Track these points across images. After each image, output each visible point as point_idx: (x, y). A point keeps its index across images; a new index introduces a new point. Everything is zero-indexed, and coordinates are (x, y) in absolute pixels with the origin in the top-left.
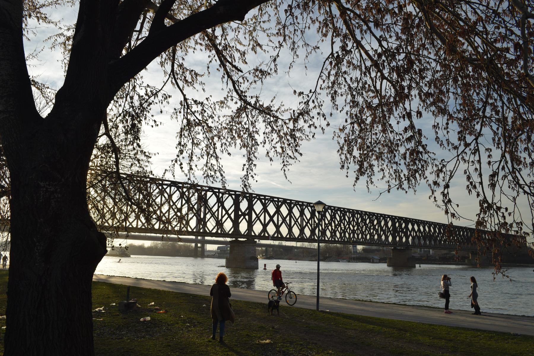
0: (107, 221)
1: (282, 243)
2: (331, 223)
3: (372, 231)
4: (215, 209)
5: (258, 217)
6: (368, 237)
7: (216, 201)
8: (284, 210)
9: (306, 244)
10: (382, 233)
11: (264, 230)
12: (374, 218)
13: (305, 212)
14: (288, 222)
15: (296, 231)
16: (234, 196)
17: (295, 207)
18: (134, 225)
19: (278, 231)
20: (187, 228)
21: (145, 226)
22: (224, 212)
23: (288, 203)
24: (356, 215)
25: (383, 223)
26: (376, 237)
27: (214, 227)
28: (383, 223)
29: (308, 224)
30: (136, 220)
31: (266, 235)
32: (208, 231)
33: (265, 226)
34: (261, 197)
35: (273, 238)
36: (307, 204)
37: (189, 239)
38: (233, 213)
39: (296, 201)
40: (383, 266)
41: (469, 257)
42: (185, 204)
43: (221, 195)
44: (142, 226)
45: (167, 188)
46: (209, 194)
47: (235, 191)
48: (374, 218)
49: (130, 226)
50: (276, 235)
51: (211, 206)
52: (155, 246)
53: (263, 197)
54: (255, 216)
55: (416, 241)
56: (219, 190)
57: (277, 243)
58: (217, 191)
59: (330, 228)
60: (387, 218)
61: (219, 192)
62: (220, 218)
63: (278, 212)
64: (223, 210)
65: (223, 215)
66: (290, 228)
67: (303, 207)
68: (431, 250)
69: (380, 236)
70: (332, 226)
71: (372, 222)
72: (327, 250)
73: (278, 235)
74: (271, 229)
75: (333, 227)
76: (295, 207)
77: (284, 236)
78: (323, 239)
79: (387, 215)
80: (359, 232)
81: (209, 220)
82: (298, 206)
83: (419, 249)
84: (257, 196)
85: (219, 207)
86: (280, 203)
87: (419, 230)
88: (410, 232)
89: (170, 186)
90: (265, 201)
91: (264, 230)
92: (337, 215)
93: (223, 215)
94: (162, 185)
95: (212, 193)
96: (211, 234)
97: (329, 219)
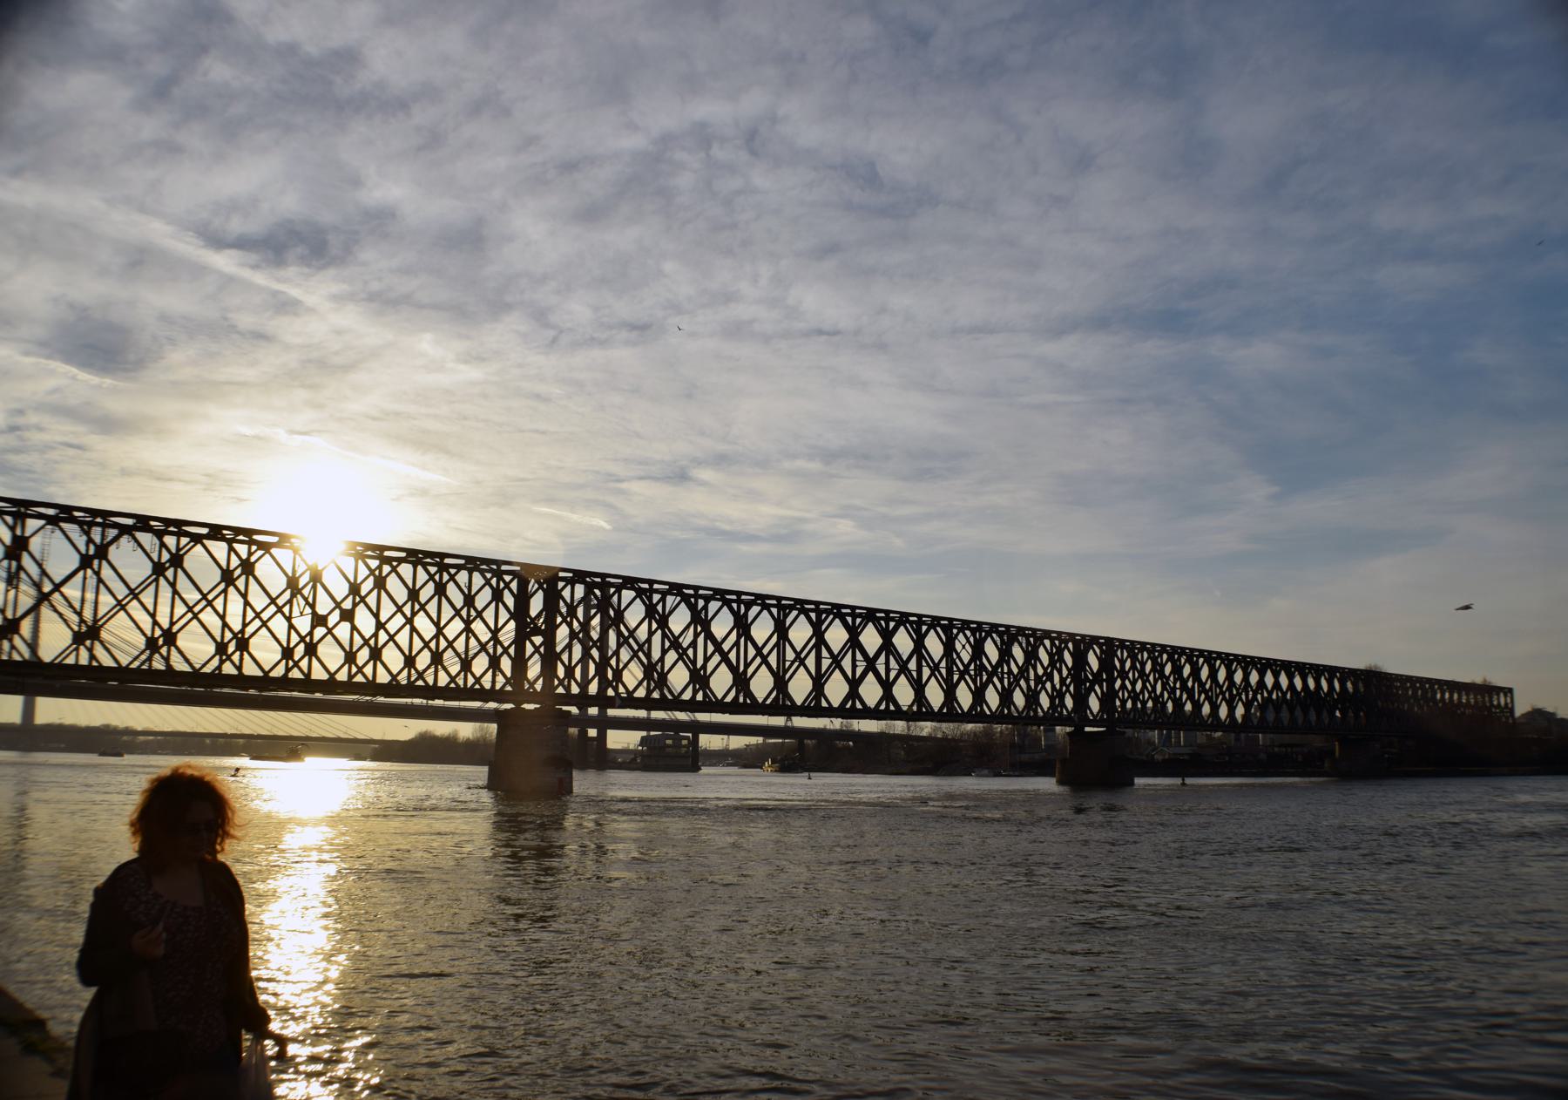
0: (360, 670)
1: (852, 725)
3: (1178, 692)
4: (642, 634)
6: (1150, 704)
8: (903, 641)
9: (899, 726)
11: (853, 694)
12: (1183, 661)
13: (461, 598)
15: (935, 695)
16: (813, 615)
17: (932, 631)
18: (487, 682)
19: (888, 696)
20: (616, 689)
22: (711, 648)
23: (911, 623)
24: (1119, 653)
25: (1205, 673)
26: (1188, 707)
28: (1205, 673)
29: (995, 680)
30: (307, 657)
31: (859, 706)
32: (988, 713)
33: (854, 683)
34: (844, 611)
38: (814, 650)
39: (934, 618)
40: (1047, 784)
41: (1333, 753)
42: (656, 630)
45: (511, 581)
46: (628, 595)
47: (779, 599)
48: (1183, 661)
49: (420, 683)
50: (883, 707)
51: (633, 625)
52: (482, 736)
53: (849, 611)
54: (843, 663)
55: (1271, 716)
56: (651, 586)
58: (692, 592)
59: (1048, 685)
60: (1198, 657)
62: (742, 668)
63: (888, 647)
65: (734, 651)
66: (919, 687)
67: (980, 635)
68: (1260, 735)
69: (1197, 706)
70: (1027, 680)
71: (1177, 670)
72: (974, 741)
73: (887, 706)
74: (871, 692)
75: (1032, 684)
76: (932, 631)
77: (799, 703)
78: (1032, 714)
80: (1126, 695)
82: (938, 629)
83: (1233, 735)
86: (892, 624)
88: (1270, 693)
89: (571, 582)
90: (854, 622)
91: (853, 694)
93: (709, 654)
95: (720, 603)
96: (630, 701)
97: (1046, 663)
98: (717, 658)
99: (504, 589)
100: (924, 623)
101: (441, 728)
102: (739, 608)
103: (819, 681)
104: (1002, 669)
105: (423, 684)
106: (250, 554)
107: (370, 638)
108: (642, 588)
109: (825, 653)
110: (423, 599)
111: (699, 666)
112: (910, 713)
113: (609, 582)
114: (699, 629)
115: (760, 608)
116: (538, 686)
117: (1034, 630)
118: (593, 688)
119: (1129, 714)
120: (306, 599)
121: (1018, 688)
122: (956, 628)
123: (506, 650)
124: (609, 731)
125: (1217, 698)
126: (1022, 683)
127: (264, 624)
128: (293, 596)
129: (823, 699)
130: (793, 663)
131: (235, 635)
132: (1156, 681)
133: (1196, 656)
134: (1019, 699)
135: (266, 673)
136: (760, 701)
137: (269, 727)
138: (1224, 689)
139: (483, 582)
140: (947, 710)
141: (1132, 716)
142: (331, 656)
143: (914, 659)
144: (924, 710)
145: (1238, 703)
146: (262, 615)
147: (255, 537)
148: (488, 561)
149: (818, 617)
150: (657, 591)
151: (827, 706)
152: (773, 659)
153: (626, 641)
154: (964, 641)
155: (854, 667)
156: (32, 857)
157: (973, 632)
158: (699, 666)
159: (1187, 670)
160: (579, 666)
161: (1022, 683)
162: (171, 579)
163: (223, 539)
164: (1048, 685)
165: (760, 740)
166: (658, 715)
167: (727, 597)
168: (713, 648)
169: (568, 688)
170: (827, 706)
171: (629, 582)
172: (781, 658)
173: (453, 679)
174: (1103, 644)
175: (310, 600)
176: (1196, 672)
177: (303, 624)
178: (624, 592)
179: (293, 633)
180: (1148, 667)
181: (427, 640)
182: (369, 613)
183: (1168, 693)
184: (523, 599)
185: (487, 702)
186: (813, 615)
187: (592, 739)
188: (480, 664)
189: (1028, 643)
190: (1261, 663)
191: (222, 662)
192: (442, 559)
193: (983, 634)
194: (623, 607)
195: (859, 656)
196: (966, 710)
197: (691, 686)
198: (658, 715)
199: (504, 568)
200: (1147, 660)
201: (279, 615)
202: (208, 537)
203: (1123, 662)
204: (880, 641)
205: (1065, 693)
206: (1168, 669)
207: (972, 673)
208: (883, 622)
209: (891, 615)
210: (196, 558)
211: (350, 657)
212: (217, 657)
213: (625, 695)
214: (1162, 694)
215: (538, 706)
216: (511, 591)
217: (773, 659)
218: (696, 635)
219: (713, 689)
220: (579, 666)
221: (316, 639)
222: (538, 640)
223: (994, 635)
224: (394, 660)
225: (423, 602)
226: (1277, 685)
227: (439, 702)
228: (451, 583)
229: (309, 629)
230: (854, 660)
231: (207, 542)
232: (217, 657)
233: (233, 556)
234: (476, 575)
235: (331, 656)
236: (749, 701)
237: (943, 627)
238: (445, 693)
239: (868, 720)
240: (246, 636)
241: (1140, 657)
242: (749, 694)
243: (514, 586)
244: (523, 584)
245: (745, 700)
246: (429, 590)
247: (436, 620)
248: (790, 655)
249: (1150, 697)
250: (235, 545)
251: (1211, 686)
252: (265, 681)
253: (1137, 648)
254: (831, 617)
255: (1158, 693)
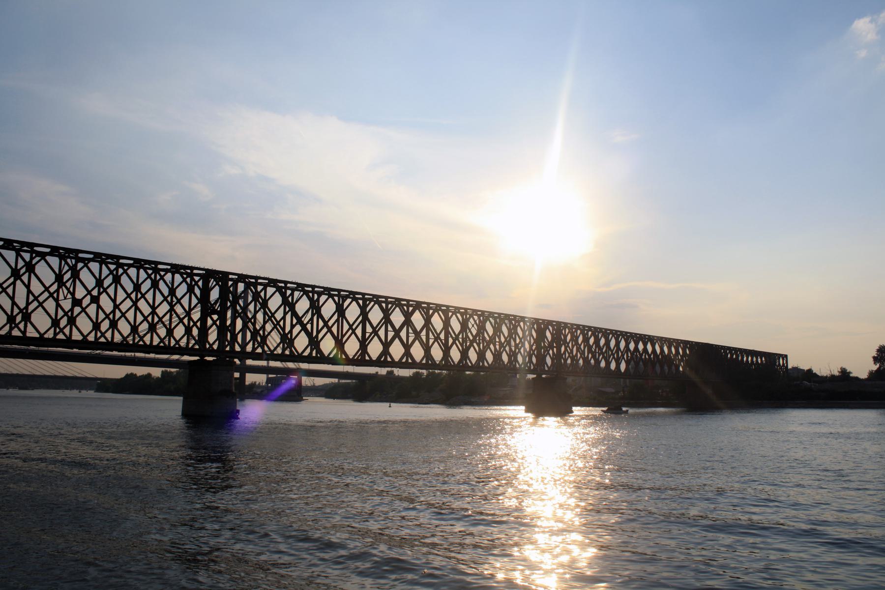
2: (510, 341)
4: (279, 315)
5: (375, 332)
6: (569, 361)
7: (280, 302)
10: (590, 356)
11: (386, 352)
12: (600, 335)
14: (424, 338)
16: (361, 302)
17: (436, 313)
18: (183, 343)
19: (407, 353)
21: (164, 343)
22: (321, 324)
25: (602, 342)
27: (278, 345)
30: (140, 283)
32: (470, 365)
33: (386, 345)
35: (378, 363)
36: (436, 307)
37: (344, 380)
38: (361, 325)
39: (456, 308)
43: (316, 297)
44: (160, 343)
46: (270, 290)
49: (141, 343)
50: (404, 360)
53: (361, 296)
54: (348, 327)
56: (256, 280)
57: (383, 371)
58: (310, 289)
59: (507, 348)
61: (287, 288)
62: (315, 334)
63: (408, 322)
64: (320, 320)
66: (427, 348)
69: (598, 362)
74: (396, 351)
75: (498, 347)
76: (436, 313)
79: (587, 326)
81: (269, 333)
82: (440, 312)
83: (622, 380)
84: (350, 294)
85: (313, 315)
86: (411, 309)
87: (636, 348)
90: (387, 306)
91: (386, 352)
92: (519, 328)
93: (320, 328)
94: (255, 285)
95: (275, 289)
98: (298, 328)
99: (159, 280)
100: (431, 308)
101: (140, 371)
102: (313, 296)
103: (364, 343)
104: (479, 338)
105: (143, 344)
106: (32, 258)
107: (110, 314)
108: (280, 286)
109: (390, 328)
110: (143, 290)
111: (287, 332)
112: (441, 365)
113: (381, 301)
114: (287, 309)
115: (327, 296)
116: (215, 347)
117: (515, 316)
118: (249, 348)
119: (569, 368)
120: (68, 289)
121: (489, 350)
122: (451, 312)
123: (195, 324)
124: (247, 374)
125: (609, 358)
126: (492, 346)
127: (41, 304)
128: (59, 287)
129: (366, 355)
130: (371, 334)
131: (21, 311)
132: (573, 347)
133: (586, 330)
134: (489, 357)
135: (42, 335)
136: (351, 357)
137: (30, 369)
138: (614, 352)
139: (181, 280)
140: (410, 363)
141: (571, 368)
142: (84, 324)
143: (424, 331)
144: (430, 362)
145: (622, 360)
146: (39, 299)
147: (36, 248)
148: (185, 267)
149: (364, 303)
150: (261, 284)
151: (369, 359)
152: (334, 329)
153: (270, 319)
154: (473, 323)
155: (408, 337)
156: (184, 444)
157: (462, 314)
158: (287, 332)
159: (592, 341)
160: (241, 333)
161: (492, 346)
162: (26, 282)
163: (13, 249)
164: (507, 348)
165: (336, 380)
166: (273, 364)
167: (332, 293)
168: (296, 321)
169: (233, 347)
170: (369, 359)
171: (273, 282)
172: (340, 328)
173: (162, 340)
174: (554, 325)
175: (71, 290)
176: (597, 341)
177: (67, 305)
178: (268, 289)
179: (60, 310)
180: (569, 337)
181: (146, 315)
182: (109, 299)
183: (580, 353)
184: (206, 291)
185: (183, 356)
186: (361, 302)
187: (236, 379)
188: (179, 331)
189: (496, 322)
190: (627, 336)
191: (11, 329)
192: (118, 260)
193: (468, 316)
194: (267, 298)
195: (390, 328)
196: (456, 363)
197: (309, 347)
198: (273, 364)
199: (195, 271)
200: (568, 334)
201: (36, 295)
202: (50, 254)
203: (566, 336)
204: (403, 319)
205: (518, 353)
206: (580, 339)
207: (461, 340)
208: (405, 308)
209: (411, 303)
210: (41, 269)
211: (96, 326)
212: (8, 325)
213: (269, 352)
214: (577, 354)
215: (215, 358)
216: (199, 287)
217: (334, 329)
218: (285, 313)
219: (296, 347)
220: (241, 333)
221: (75, 314)
222: (215, 317)
223: (491, 319)
224: (124, 327)
225: (143, 292)
226: (645, 350)
227: (152, 355)
228: (125, 275)
229: (70, 307)
230: (408, 333)
231: (48, 258)
232: (8, 325)
233: (20, 260)
234: (142, 271)
235: (84, 324)
236: (319, 355)
237: (443, 311)
238: (157, 349)
239: (374, 367)
240: (29, 311)
241: (563, 332)
242: (319, 351)
243: (200, 283)
244: (206, 283)
245: (316, 354)
246: (147, 284)
247: (138, 312)
248: (369, 329)
249: (569, 356)
250: (23, 254)
251: (606, 350)
252: (41, 340)
253: (562, 326)
254: (372, 303)
255: (574, 353)
